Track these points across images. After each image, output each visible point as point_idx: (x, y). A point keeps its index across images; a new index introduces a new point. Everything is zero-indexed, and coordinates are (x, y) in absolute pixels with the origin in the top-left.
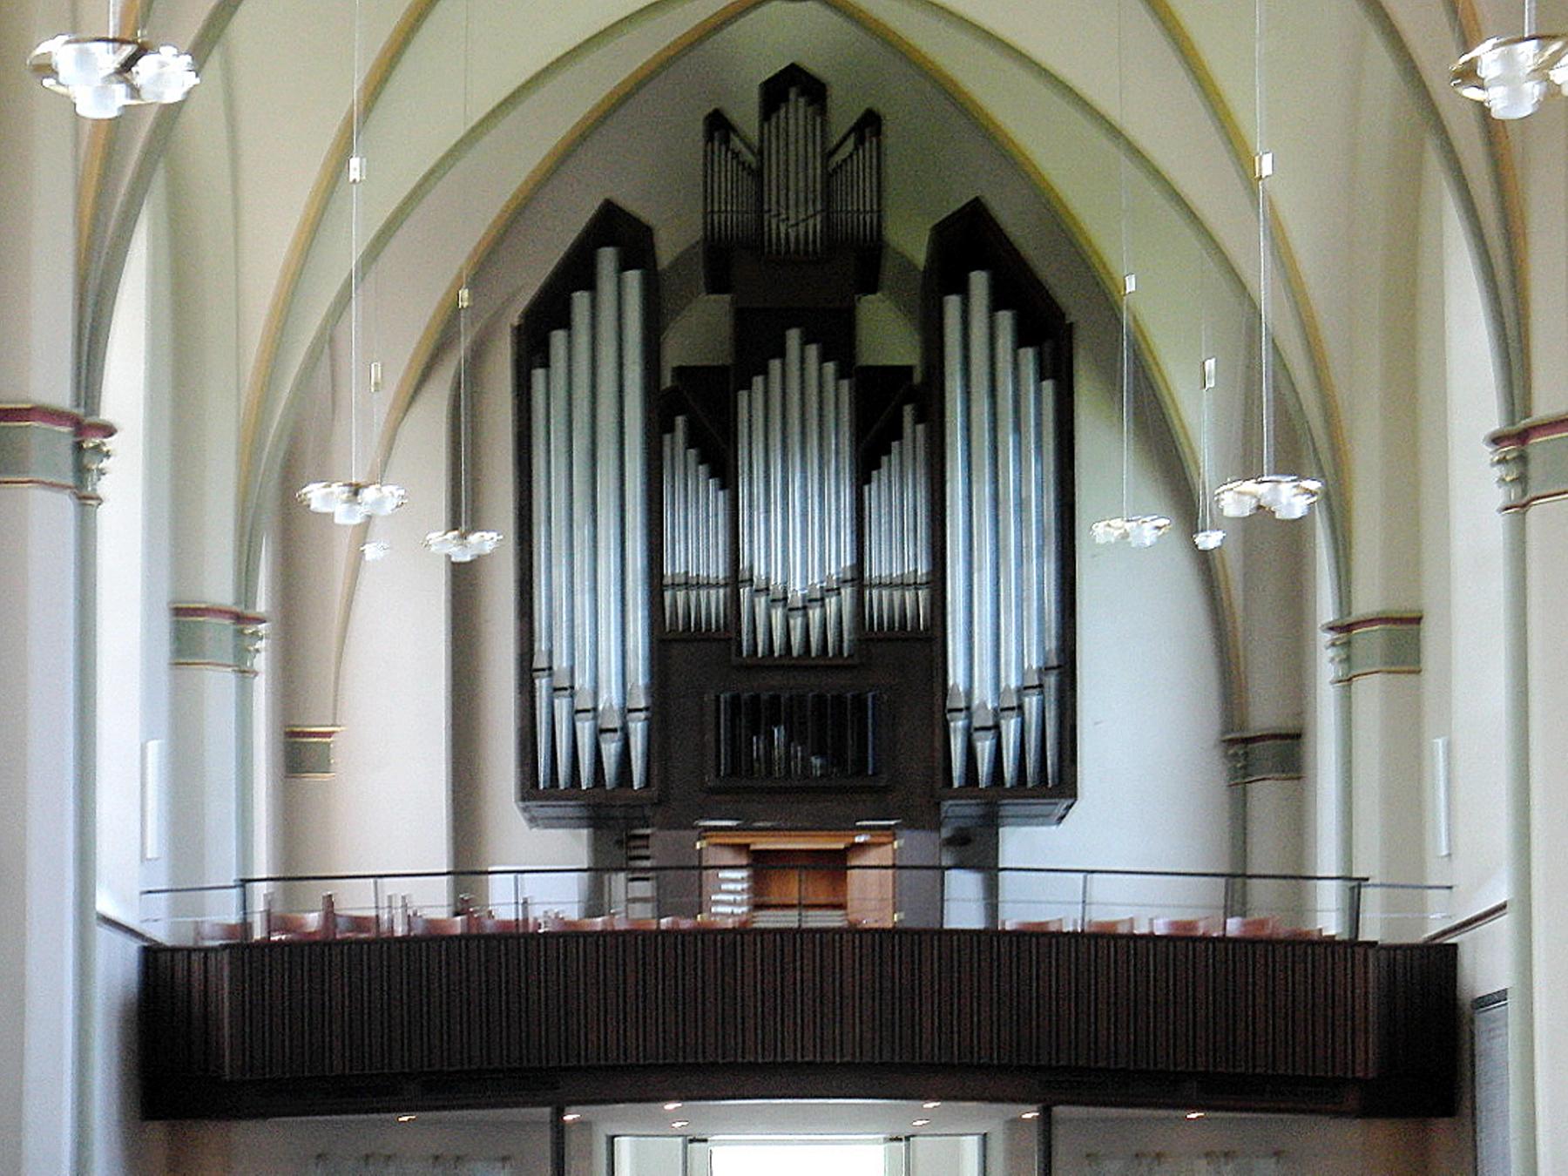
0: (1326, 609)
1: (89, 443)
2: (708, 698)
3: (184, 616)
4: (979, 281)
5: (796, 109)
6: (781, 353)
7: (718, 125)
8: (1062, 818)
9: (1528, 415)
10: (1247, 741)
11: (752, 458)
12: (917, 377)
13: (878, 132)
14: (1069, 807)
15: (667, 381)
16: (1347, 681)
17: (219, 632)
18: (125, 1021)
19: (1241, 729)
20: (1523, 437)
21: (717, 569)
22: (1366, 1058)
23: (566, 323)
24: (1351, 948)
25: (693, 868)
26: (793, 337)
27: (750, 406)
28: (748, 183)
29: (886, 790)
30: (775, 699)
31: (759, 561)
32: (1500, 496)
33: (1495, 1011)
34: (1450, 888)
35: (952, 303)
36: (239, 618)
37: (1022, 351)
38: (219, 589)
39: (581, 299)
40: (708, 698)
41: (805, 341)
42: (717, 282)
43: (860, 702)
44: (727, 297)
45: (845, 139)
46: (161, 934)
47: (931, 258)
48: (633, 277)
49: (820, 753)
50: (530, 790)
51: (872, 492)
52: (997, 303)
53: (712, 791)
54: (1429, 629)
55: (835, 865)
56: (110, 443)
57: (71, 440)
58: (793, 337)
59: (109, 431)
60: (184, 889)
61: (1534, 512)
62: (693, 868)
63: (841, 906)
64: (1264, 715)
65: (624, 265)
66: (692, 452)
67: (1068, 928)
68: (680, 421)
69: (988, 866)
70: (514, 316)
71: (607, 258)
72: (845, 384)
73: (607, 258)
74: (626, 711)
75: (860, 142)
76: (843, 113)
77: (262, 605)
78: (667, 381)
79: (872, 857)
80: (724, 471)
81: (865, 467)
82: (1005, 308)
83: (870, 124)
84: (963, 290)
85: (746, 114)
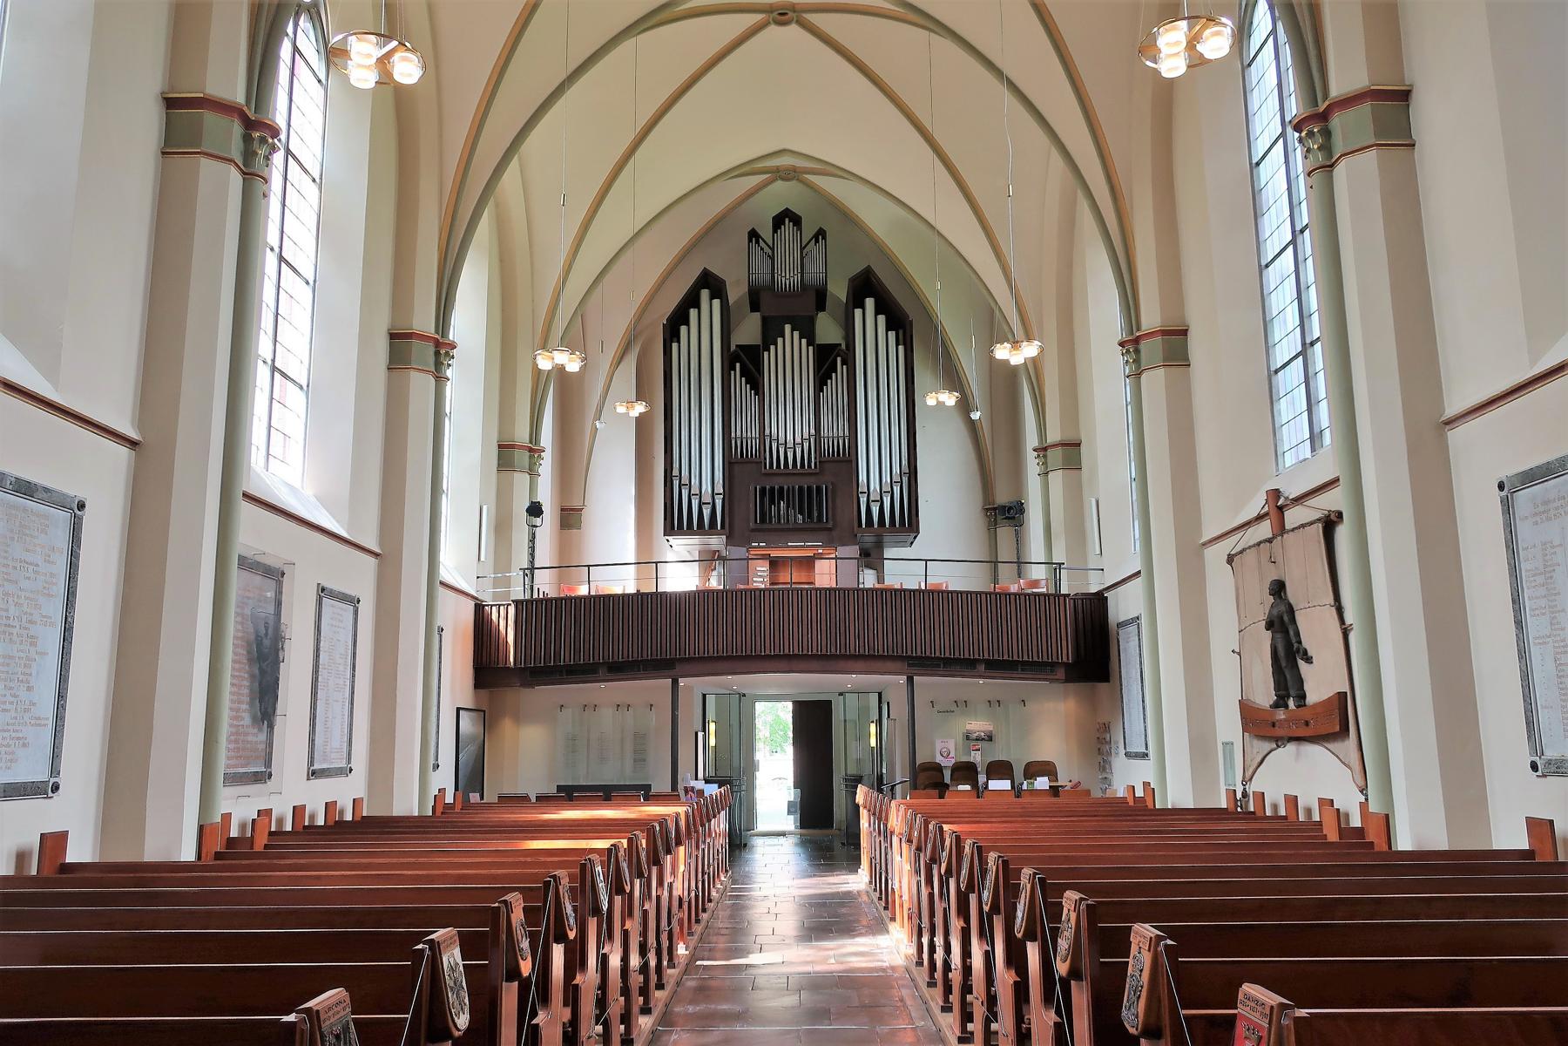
0: (1031, 440)
1: (443, 352)
3: (399, 339)
4: (870, 303)
7: (754, 235)
8: (912, 543)
9: (1138, 330)
12: (843, 347)
13: (824, 238)
14: (915, 538)
15: (733, 348)
17: (522, 458)
22: (1066, 654)
26: (788, 328)
27: (768, 358)
30: (781, 489)
32: (1037, 470)
34: (1103, 570)
35: (858, 312)
36: (531, 450)
39: (693, 313)
42: (755, 307)
43: (819, 489)
44: (759, 313)
45: (810, 241)
48: (716, 302)
52: (878, 312)
53: (753, 530)
54: (1083, 448)
55: (808, 563)
57: (434, 349)
58: (788, 328)
61: (1144, 376)
64: (1002, 497)
65: (712, 297)
68: (738, 365)
71: (705, 294)
72: (811, 348)
73: (705, 294)
75: (817, 241)
81: (821, 381)
83: (820, 234)
84: (862, 306)
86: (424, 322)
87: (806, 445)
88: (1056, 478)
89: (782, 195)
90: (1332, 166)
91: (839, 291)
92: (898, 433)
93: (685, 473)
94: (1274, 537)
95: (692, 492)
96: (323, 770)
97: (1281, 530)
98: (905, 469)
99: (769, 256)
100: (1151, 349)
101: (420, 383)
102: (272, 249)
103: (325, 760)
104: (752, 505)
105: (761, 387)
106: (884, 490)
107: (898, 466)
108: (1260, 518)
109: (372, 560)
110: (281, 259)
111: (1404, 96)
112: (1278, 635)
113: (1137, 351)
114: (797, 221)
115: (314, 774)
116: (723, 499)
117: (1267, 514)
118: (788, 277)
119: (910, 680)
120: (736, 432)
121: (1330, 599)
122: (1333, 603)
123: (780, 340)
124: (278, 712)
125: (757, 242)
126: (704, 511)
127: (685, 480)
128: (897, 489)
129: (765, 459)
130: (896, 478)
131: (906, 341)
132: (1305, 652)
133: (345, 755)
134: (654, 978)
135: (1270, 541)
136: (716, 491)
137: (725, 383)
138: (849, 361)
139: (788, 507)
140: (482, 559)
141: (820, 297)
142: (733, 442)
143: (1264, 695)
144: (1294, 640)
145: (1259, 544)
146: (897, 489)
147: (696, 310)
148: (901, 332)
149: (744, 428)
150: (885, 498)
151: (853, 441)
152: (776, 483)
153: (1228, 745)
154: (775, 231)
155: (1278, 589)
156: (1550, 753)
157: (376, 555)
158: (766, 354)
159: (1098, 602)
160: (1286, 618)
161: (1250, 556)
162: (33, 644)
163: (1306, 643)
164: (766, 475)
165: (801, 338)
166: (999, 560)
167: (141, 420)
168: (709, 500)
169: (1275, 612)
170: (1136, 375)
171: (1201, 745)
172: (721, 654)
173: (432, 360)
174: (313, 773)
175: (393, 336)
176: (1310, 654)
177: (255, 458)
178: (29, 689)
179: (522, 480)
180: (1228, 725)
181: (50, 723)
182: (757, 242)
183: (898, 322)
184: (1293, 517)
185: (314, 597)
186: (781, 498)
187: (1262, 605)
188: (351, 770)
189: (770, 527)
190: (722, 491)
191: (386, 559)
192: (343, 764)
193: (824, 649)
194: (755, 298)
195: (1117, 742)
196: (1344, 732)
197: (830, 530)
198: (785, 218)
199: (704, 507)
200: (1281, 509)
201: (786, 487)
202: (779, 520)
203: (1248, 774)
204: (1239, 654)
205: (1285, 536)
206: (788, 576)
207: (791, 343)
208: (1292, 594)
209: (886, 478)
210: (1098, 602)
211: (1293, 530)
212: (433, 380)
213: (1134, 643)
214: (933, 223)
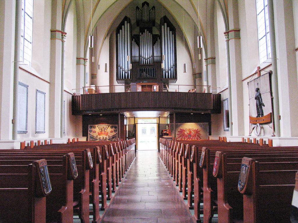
0: (204, 57)
1: (63, 35)
2: (137, 69)
3: (78, 59)
4: (166, 24)
7: (137, 8)
11: (141, 44)
15: (133, 35)
17: (82, 61)
20: (207, 59)
24: (209, 94)
26: (146, 30)
32: (225, 39)
33: (226, 101)
36: (84, 59)
37: (170, 32)
39: (123, 26)
40: (137, 69)
41: (147, 31)
48: (128, 24)
50: (117, 79)
52: (167, 26)
55: (151, 86)
58: (146, 30)
59: (87, 60)
60: (78, 89)
66: (136, 44)
68: (134, 39)
71: (126, 22)
75: (153, 9)
76: (151, 6)
80: (138, 45)
81: (154, 44)
83: (154, 7)
85: (140, 6)
86: (59, 27)
87: (150, 59)
88: (210, 67)
90: (229, 41)
94: (258, 77)
100: (231, 34)
102: (23, 10)
106: (169, 69)
107: (172, 63)
108: (255, 73)
110: (25, 12)
111: (239, 31)
113: (228, 35)
114: (148, 4)
117: (257, 72)
118: (146, 18)
121: (269, 90)
122: (270, 91)
125: (138, 9)
130: (172, 66)
131: (174, 33)
132: (263, 104)
133: (43, 129)
134: (115, 184)
141: (153, 23)
143: (255, 115)
144: (261, 101)
150: (169, 71)
154: (142, 7)
155: (258, 90)
157: (49, 83)
159: (219, 96)
160: (259, 96)
161: (253, 82)
163: (263, 102)
164: (141, 66)
165: (149, 33)
170: (228, 41)
176: (264, 104)
177: (20, 59)
179: (82, 67)
182: (138, 9)
184: (262, 73)
185: (35, 92)
187: (254, 94)
188: (45, 132)
191: (51, 83)
192: (43, 131)
194: (138, 23)
196: (271, 122)
205: (261, 77)
206: (147, 89)
208: (261, 91)
210: (219, 96)
211: (262, 75)
212: (84, 66)
213: (226, 104)
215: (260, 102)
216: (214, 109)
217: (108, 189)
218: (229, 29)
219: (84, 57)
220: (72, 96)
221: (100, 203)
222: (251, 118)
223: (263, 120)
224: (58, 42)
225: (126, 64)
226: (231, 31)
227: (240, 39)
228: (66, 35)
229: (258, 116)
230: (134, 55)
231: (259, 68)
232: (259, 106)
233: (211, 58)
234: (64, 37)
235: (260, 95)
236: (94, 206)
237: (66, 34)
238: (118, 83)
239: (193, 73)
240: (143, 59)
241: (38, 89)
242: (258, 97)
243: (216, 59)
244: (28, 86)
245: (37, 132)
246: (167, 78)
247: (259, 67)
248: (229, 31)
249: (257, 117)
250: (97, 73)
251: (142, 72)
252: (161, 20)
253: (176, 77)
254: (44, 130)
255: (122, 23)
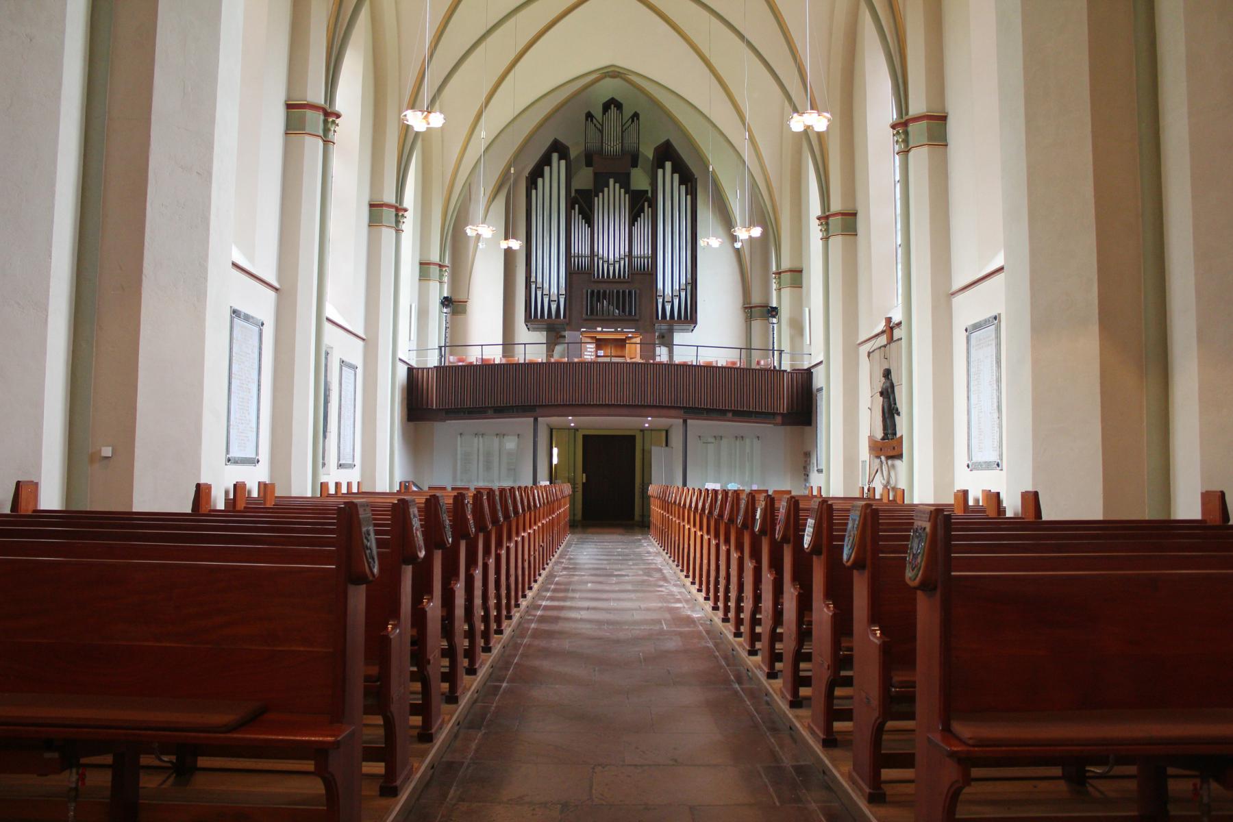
1: (400, 214)
4: (668, 165)
5: (613, 110)
6: (608, 186)
7: (589, 116)
10: (751, 308)
11: (598, 217)
13: (638, 119)
14: (695, 327)
15: (573, 194)
16: (779, 290)
17: (435, 270)
18: (403, 390)
19: (750, 304)
20: (827, 217)
21: (587, 252)
22: (784, 407)
23: (542, 176)
25: (644, 344)
26: (611, 181)
27: (598, 202)
28: (600, 134)
29: (637, 320)
30: (605, 292)
31: (601, 250)
32: (820, 235)
35: (660, 172)
36: (440, 266)
37: (681, 186)
38: (435, 257)
39: (547, 169)
40: (584, 291)
41: (615, 182)
42: (589, 163)
43: (630, 293)
46: (414, 364)
47: (653, 158)
48: (563, 163)
49: (618, 309)
51: (635, 229)
52: (674, 171)
53: (586, 320)
55: (621, 344)
56: (406, 214)
57: (394, 213)
58: (611, 181)
59: (406, 210)
60: (422, 350)
62: (644, 344)
63: (624, 357)
65: (560, 158)
67: (719, 365)
68: (577, 206)
69: (670, 345)
70: (526, 173)
71: (555, 156)
72: (627, 196)
73: (555, 156)
74: (558, 295)
75: (633, 121)
76: (628, 112)
77: (447, 262)
78: (573, 194)
79: (634, 340)
81: (633, 221)
82: (677, 173)
83: (636, 116)
84: (663, 167)
85: (597, 112)
86: (390, 197)
87: (622, 263)
89: (609, 89)
90: (908, 151)
91: (648, 152)
92: (685, 255)
93: (539, 280)
95: (544, 293)
96: (344, 464)
97: (891, 340)
98: (689, 280)
99: (599, 130)
101: (388, 234)
103: (344, 459)
104: (584, 303)
105: (592, 222)
106: (674, 294)
109: (360, 343)
111: (944, 118)
112: (885, 400)
114: (619, 106)
115: (340, 466)
116: (565, 298)
118: (612, 145)
119: (685, 421)
120: (575, 250)
123: (606, 189)
124: (328, 430)
125: (592, 121)
126: (552, 306)
127: (539, 285)
128: (683, 294)
129: (594, 271)
130: (683, 287)
133: (352, 457)
135: (885, 346)
136: (560, 293)
137: (568, 217)
138: (653, 204)
139: (609, 304)
140: (412, 338)
141: (634, 160)
142: (573, 259)
143: (879, 434)
144: (892, 403)
145: (880, 348)
146: (683, 294)
147: (549, 167)
148: (689, 185)
149: (581, 247)
150: (675, 301)
151: (654, 260)
152: (602, 287)
153: (864, 462)
154: (604, 113)
155: (887, 374)
156: (974, 460)
157: (363, 340)
158: (596, 199)
159: (808, 373)
160: (889, 390)
162: (249, 392)
164: (595, 282)
165: (620, 188)
166: (752, 347)
167: (280, 278)
168: (556, 298)
169: (884, 387)
171: (850, 462)
172: (565, 403)
173: (393, 219)
174: (340, 465)
175: (371, 206)
176: (899, 410)
178: (249, 414)
180: (864, 453)
181: (255, 430)
182: (592, 121)
183: (688, 179)
186: (604, 298)
187: (880, 383)
189: (596, 318)
190: (564, 293)
193: (667, 403)
194: (589, 158)
195: (813, 464)
197: (637, 320)
198: (612, 104)
199: (552, 303)
200: (892, 329)
201: (608, 291)
202: (603, 314)
203: (871, 479)
204: (871, 410)
207: (614, 190)
208: (894, 377)
209: (676, 287)
210: (808, 373)
214: (708, 116)
215: (890, 406)
216: (789, 413)
217: (470, 642)
218: (829, 211)
219: (440, 261)
220: (408, 368)
221: (443, 680)
222: (871, 439)
223: (892, 448)
224: (314, 146)
225: (553, 279)
226: (917, 119)
227: (947, 145)
228: (337, 121)
229: (886, 437)
230: (576, 251)
231: (889, 320)
232: (889, 413)
233: (791, 271)
234: (332, 129)
235: (892, 386)
236: (389, 725)
237: (338, 116)
238: (528, 329)
239: (744, 304)
240: (601, 262)
241: (344, 359)
242: (888, 392)
243: (803, 272)
244: (263, 324)
245: (340, 465)
246: (668, 318)
247: (890, 318)
248: (907, 117)
249: (883, 439)
250: (468, 299)
251: (598, 300)
252: (657, 150)
253: (694, 318)
254: (354, 461)
255: (546, 160)
